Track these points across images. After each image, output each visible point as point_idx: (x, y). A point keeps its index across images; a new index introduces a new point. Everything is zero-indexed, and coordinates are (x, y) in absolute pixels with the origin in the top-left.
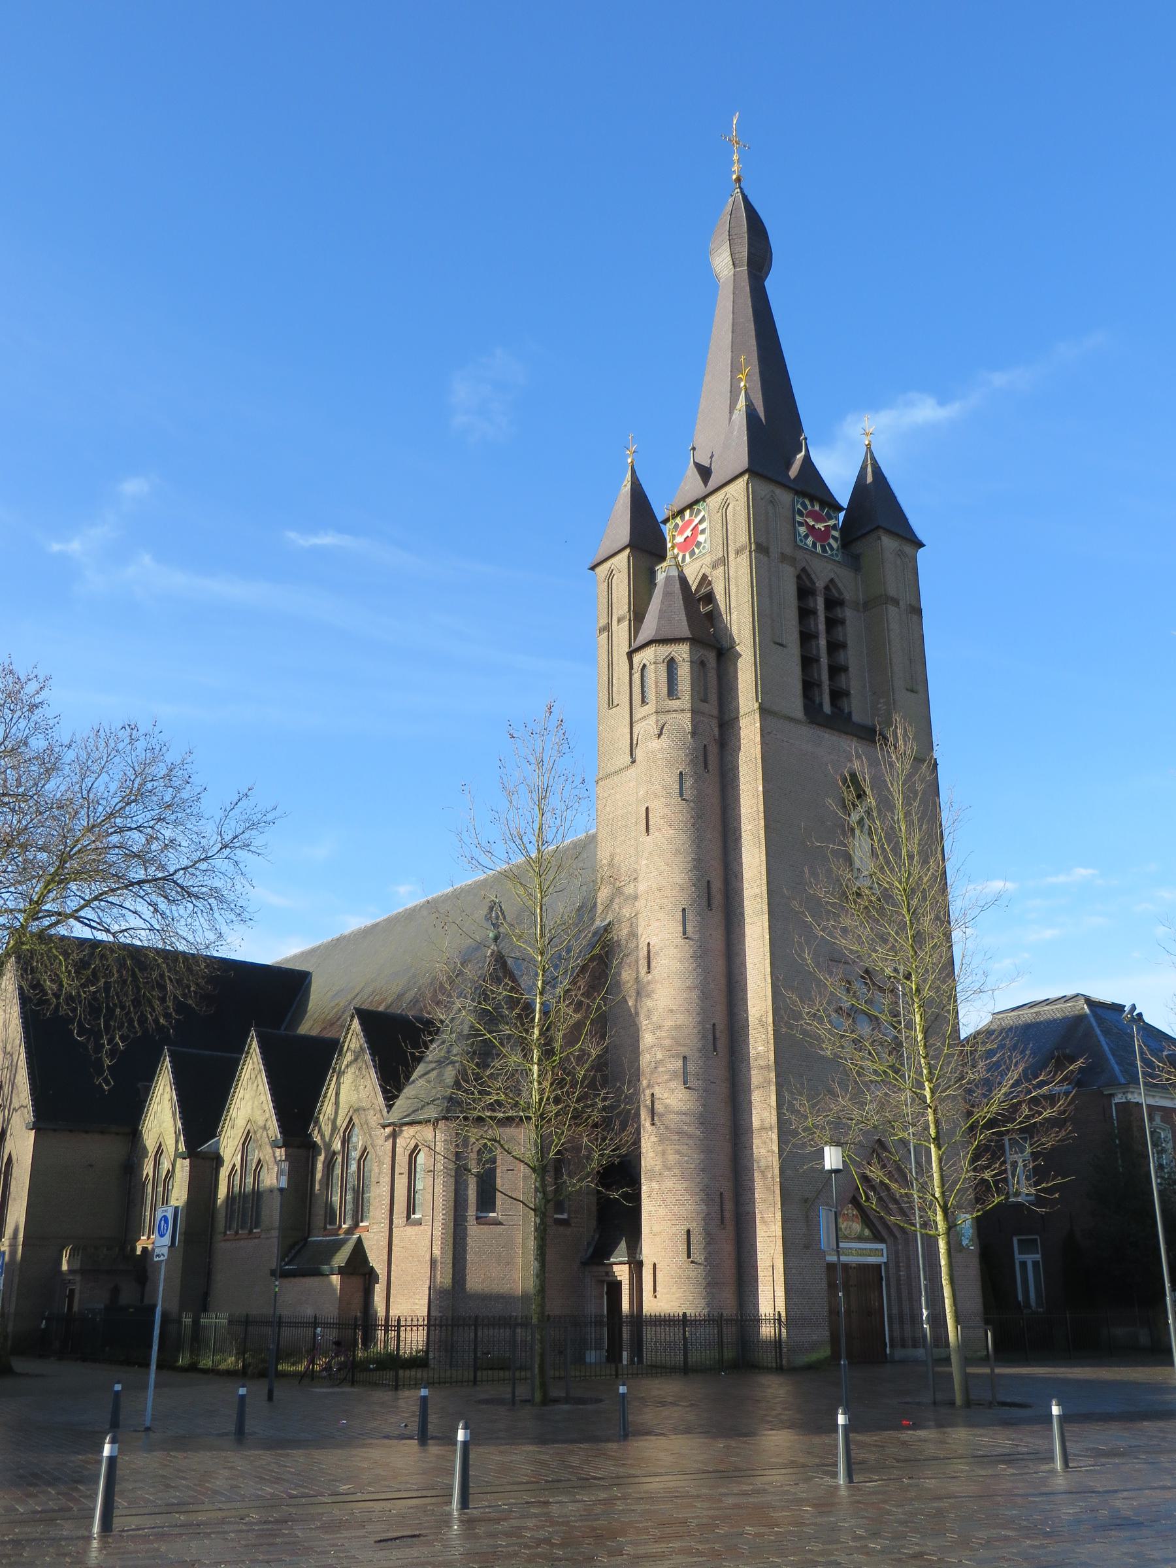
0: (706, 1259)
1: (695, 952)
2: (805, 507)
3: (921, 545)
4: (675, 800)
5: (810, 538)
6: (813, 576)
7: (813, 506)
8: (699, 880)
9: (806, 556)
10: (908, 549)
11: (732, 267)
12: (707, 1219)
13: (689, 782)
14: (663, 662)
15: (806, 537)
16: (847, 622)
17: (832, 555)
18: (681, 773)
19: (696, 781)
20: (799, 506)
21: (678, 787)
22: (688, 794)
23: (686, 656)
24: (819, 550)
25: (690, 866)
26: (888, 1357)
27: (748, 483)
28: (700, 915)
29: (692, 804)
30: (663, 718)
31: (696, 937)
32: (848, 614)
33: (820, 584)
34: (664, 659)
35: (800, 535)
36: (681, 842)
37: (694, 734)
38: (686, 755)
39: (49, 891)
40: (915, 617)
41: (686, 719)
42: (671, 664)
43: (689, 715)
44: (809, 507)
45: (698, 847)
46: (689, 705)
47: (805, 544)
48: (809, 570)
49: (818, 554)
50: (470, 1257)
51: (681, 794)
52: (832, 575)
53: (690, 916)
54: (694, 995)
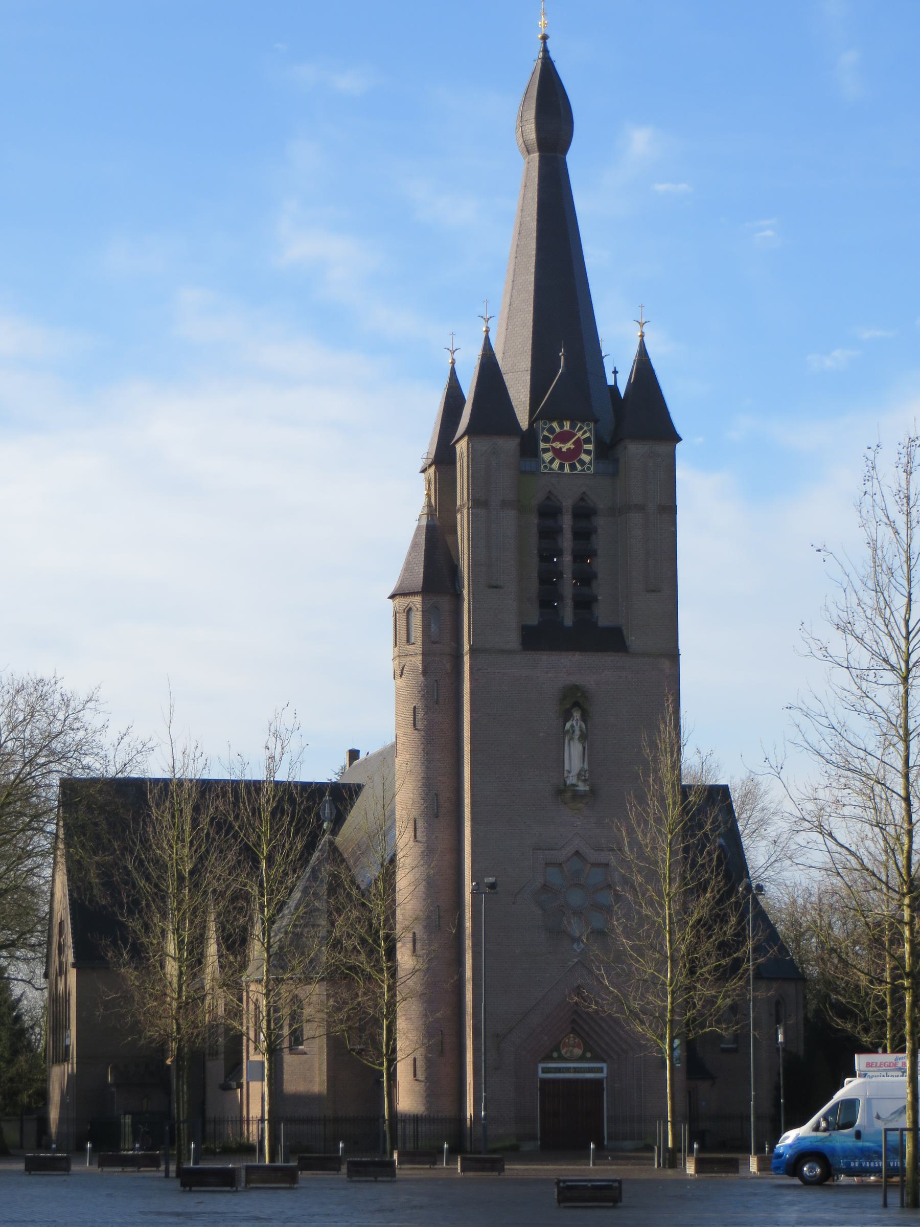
0: (426, 1078)
1: (422, 852)
2: (552, 430)
4: (410, 729)
7: (561, 426)
8: (427, 794)
11: (527, 153)
12: (429, 1049)
13: (420, 716)
14: (404, 612)
15: (552, 461)
16: (599, 530)
17: (583, 470)
18: (415, 707)
19: (426, 713)
20: (546, 433)
21: (412, 719)
22: (420, 725)
23: (419, 606)
24: (567, 469)
25: (420, 784)
26: (296, 1047)
27: (468, 444)
28: (427, 822)
29: (423, 733)
30: (404, 660)
31: (424, 840)
32: (600, 522)
33: (567, 504)
34: (405, 609)
35: (544, 462)
36: (414, 764)
37: (425, 672)
38: (419, 692)
39: (879, 599)
41: (418, 661)
42: (409, 611)
43: (420, 658)
44: (558, 430)
45: (427, 768)
46: (421, 649)
47: (551, 469)
49: (566, 474)
50: (250, 1088)
51: (415, 725)
53: (420, 824)
54: (422, 888)
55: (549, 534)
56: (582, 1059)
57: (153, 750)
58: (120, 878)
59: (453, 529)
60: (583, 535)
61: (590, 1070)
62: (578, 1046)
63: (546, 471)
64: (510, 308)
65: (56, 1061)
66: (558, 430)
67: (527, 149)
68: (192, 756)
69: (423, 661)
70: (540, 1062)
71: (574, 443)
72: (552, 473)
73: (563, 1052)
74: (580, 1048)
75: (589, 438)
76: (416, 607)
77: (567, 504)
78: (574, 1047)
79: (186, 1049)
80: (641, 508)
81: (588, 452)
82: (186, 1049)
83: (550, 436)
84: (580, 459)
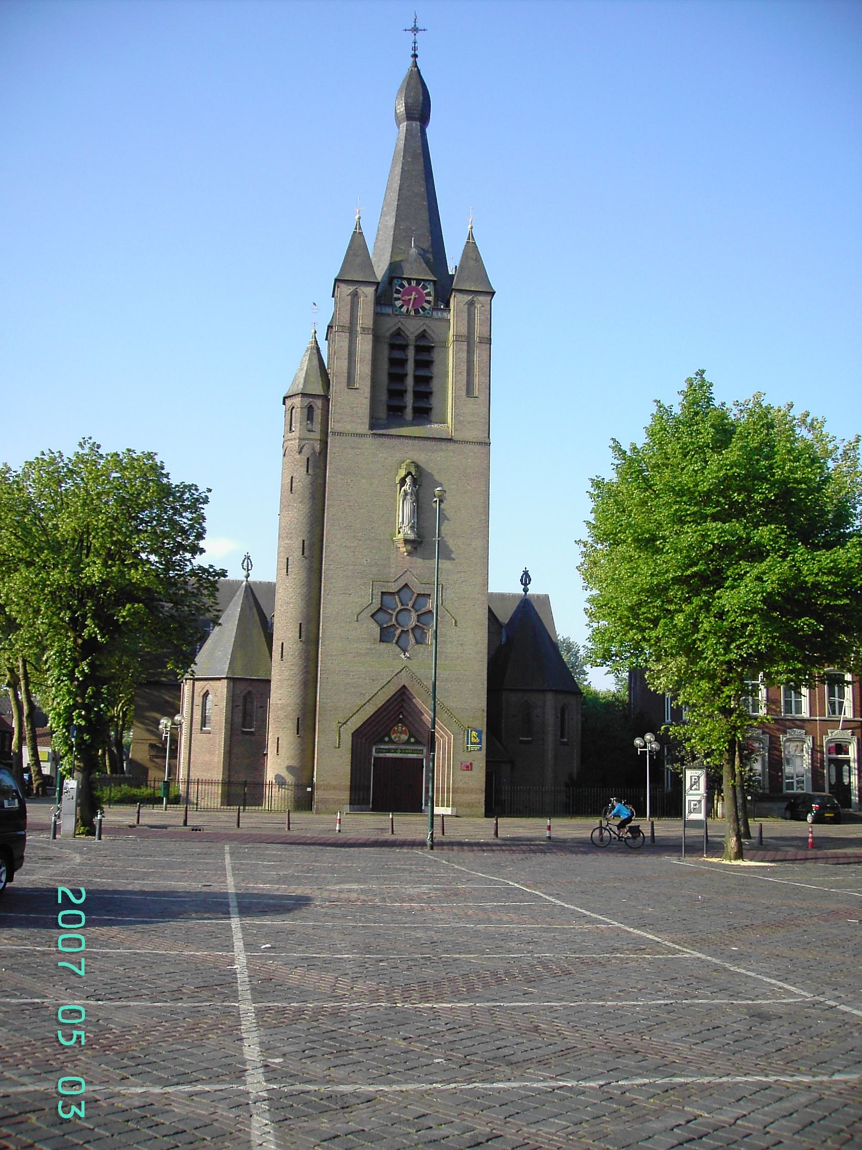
15: (402, 306)
44: (407, 286)
47: (400, 312)
55: (397, 363)
56: (407, 742)
57: (99, 447)
58: (51, 725)
60: (396, 394)
61: (413, 752)
62: (405, 733)
65: (443, 801)
66: (407, 286)
70: (374, 744)
73: (393, 737)
74: (406, 734)
75: (430, 292)
78: (401, 733)
79: (830, 516)
81: (428, 302)
82: (830, 516)
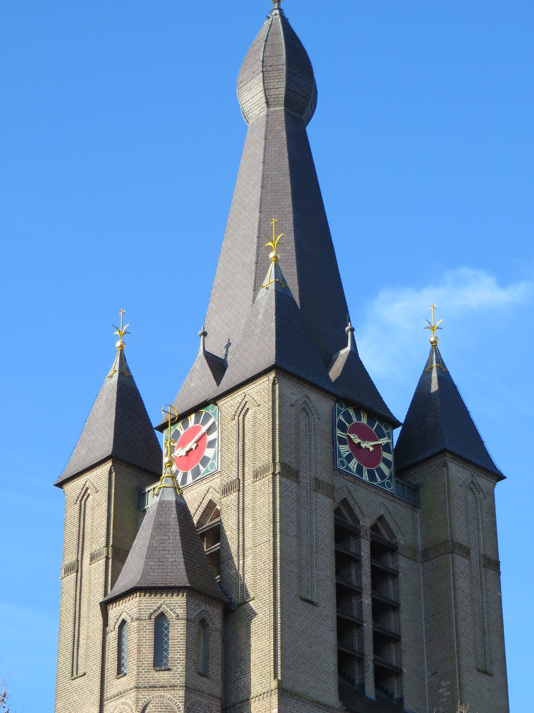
2: (349, 419)
3: (500, 477)
5: (354, 460)
6: (357, 512)
9: (348, 483)
10: (483, 481)
11: (265, 105)
23: (181, 611)
24: (365, 476)
30: (146, 696)
33: (366, 523)
34: (151, 615)
40: (491, 573)
43: (182, 693)
46: (183, 679)
47: (348, 468)
48: (352, 503)
49: (364, 482)
52: (382, 511)
59: (430, 380)
63: (342, 468)
64: (257, 267)
67: (267, 99)
68: (260, 108)
69: (187, 700)
71: (373, 446)
72: (346, 474)
76: (174, 613)
77: (366, 523)
80: (466, 552)
81: (387, 462)
83: (346, 423)
84: (379, 467)
